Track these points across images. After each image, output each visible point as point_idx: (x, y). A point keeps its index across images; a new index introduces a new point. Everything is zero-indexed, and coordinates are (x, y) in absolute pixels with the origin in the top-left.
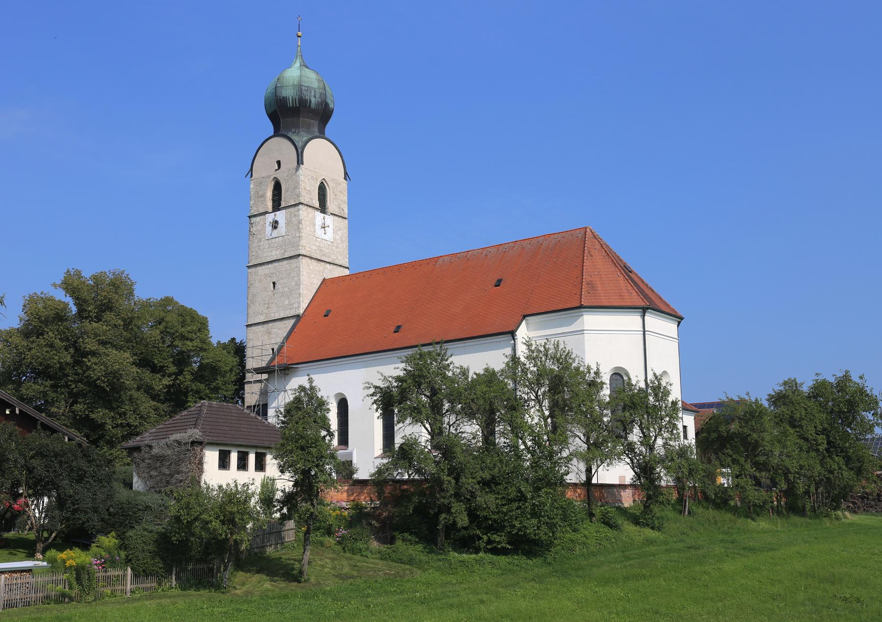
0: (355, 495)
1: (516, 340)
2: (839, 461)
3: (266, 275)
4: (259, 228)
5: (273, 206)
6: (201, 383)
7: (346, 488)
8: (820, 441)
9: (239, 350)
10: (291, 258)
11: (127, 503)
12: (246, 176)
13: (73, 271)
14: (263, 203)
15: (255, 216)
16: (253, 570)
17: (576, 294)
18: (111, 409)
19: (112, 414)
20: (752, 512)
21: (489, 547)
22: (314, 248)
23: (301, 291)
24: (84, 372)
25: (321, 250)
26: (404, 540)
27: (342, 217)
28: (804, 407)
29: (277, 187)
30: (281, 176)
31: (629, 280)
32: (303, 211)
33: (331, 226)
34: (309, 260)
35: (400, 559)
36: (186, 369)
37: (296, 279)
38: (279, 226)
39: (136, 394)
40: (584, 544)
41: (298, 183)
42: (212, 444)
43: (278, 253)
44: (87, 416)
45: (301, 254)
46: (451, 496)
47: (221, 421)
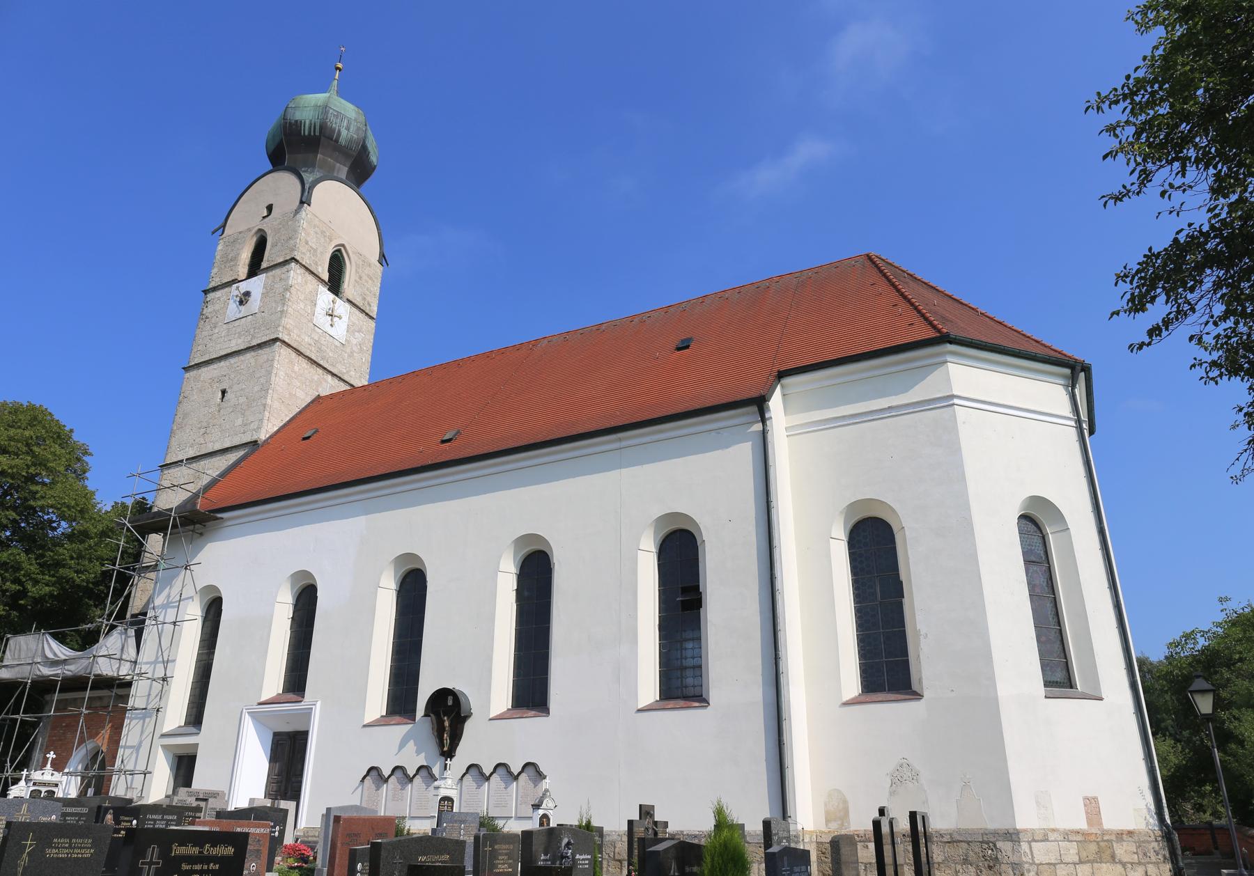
1: (768, 422)
4: (217, 307)
10: (260, 346)
14: (232, 270)
22: (307, 339)
23: (269, 401)
27: (367, 314)
30: (268, 226)
33: (345, 318)
34: (293, 355)
37: (263, 381)
38: (251, 299)
41: (296, 231)
43: (240, 341)
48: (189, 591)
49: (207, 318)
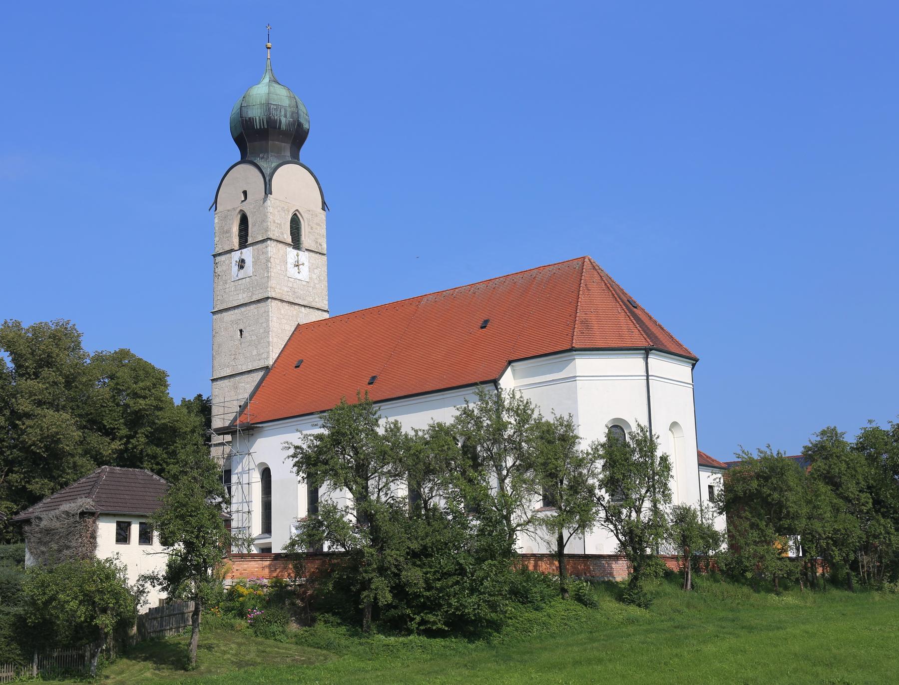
0: (278, 570)
2: (886, 524)
3: (232, 322)
4: (224, 268)
5: (239, 242)
6: (157, 446)
7: (268, 563)
8: (863, 501)
9: (204, 408)
10: (259, 301)
11: (6, 582)
12: (210, 210)
13: (11, 322)
15: (220, 254)
16: (140, 658)
17: (567, 335)
18: (52, 478)
19: (52, 484)
20: (777, 585)
21: (422, 628)
22: (286, 289)
23: (271, 340)
24: (19, 436)
25: (293, 292)
26: (326, 622)
27: (320, 253)
28: (845, 461)
29: (244, 221)
30: (248, 208)
31: (631, 317)
32: (272, 247)
33: (306, 264)
34: (279, 303)
35: (317, 644)
36: (139, 431)
37: (264, 325)
39: (80, 461)
40: (544, 624)
41: (266, 216)
42: (107, 515)
43: (245, 296)
44: (24, 487)
45: (270, 296)
46: (374, 570)
47: (122, 488)
48: (252, 466)
49: (219, 276)
